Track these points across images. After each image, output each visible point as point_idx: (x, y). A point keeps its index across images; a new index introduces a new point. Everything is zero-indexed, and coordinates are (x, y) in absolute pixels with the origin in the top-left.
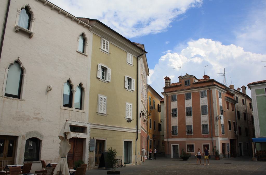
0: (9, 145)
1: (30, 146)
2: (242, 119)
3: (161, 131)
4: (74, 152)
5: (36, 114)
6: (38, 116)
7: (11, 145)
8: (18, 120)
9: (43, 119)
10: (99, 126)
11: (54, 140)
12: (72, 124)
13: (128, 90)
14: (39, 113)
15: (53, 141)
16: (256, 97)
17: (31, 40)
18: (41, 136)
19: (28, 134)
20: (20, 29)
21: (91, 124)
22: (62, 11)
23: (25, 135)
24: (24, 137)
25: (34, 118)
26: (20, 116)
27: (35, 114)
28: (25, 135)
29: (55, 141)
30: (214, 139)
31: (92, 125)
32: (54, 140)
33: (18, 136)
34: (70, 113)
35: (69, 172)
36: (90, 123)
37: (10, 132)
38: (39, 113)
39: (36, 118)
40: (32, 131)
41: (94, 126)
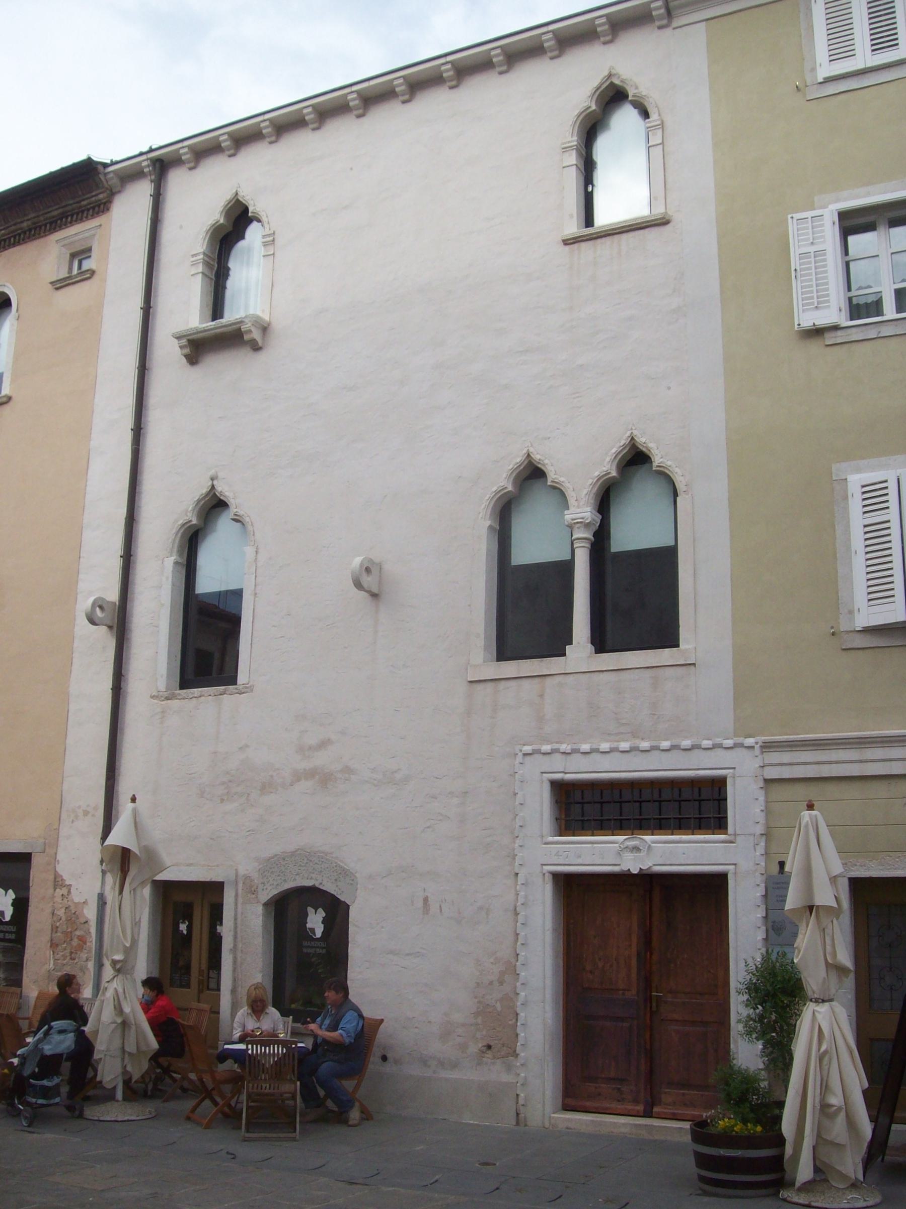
0: (190, 928)
1: (305, 934)
2: (655, 113)
3: (571, 643)
4: (647, 983)
5: (310, 748)
6: (321, 759)
7: (183, 927)
8: (222, 800)
9: (348, 770)
10: (869, 754)
11: (426, 900)
12: (569, 777)
13: (856, 335)
14: (324, 744)
15: (420, 904)
17: (13, 397)
18: (345, 873)
19: (272, 864)
20: (189, 340)
21: (767, 747)
22: (606, 15)
23: (255, 875)
24: (251, 887)
25: (298, 777)
26: (228, 773)
27: (303, 750)
28: (255, 875)
29: (434, 908)
31: (774, 757)
32: (426, 900)
33: (219, 879)
34: (541, 696)
35: (550, 1117)
36: (750, 741)
37: (191, 865)
38: (324, 744)
39: (310, 774)
40: (291, 848)
41: (786, 757)
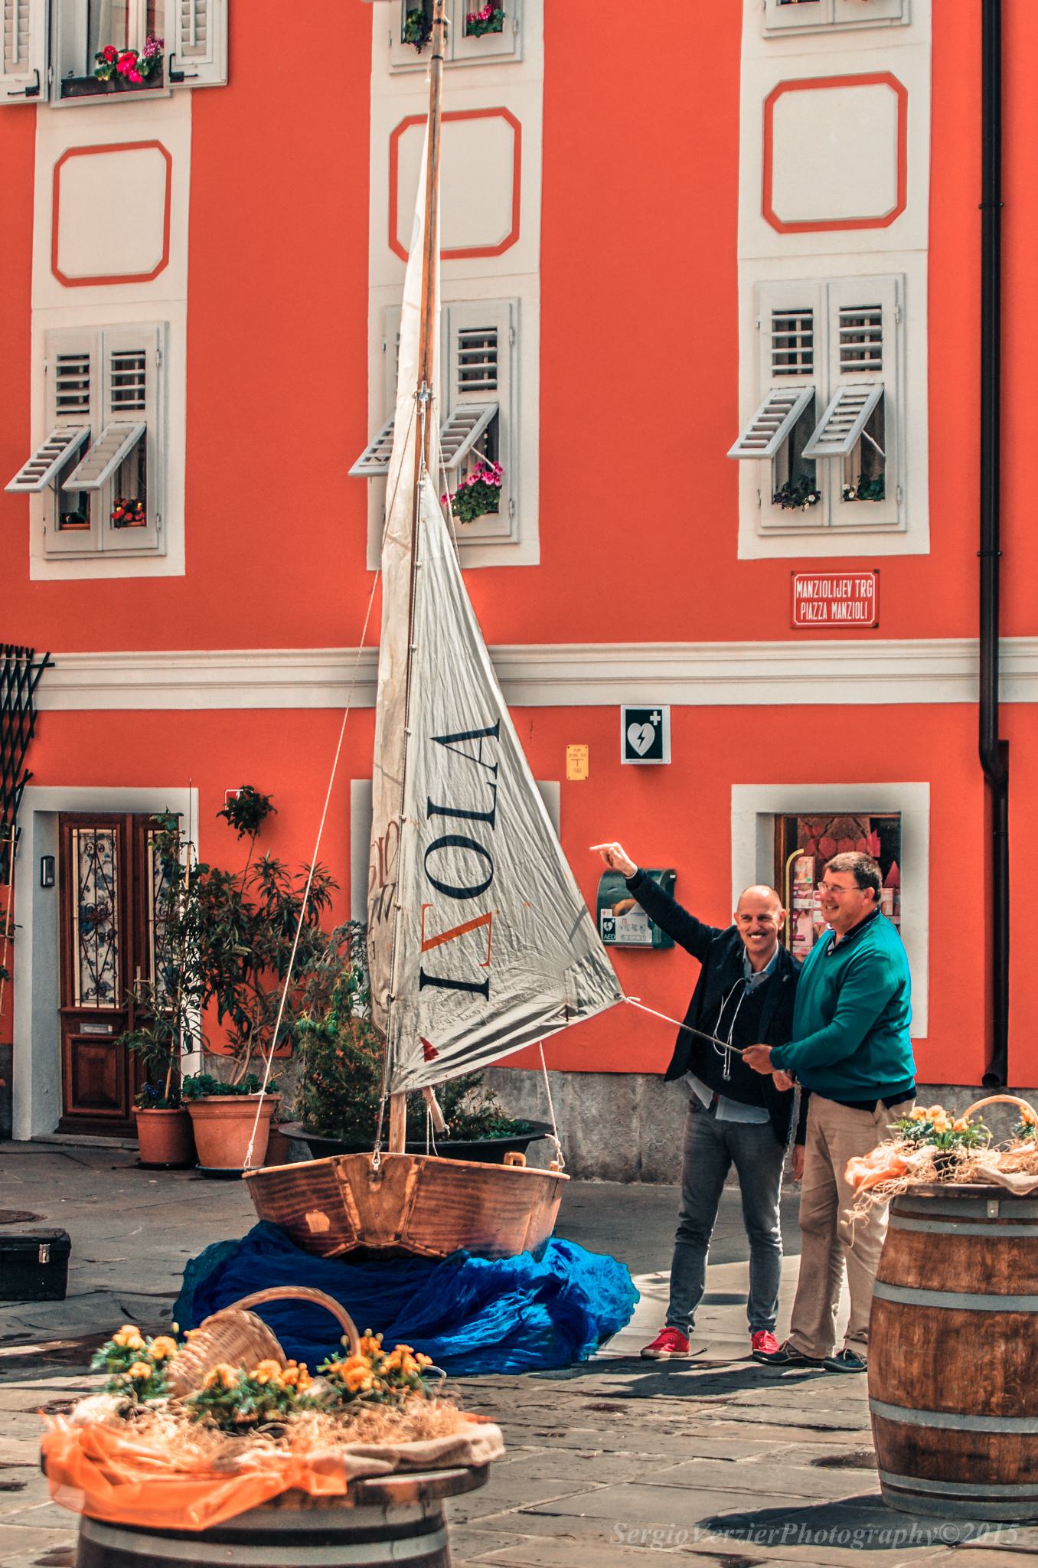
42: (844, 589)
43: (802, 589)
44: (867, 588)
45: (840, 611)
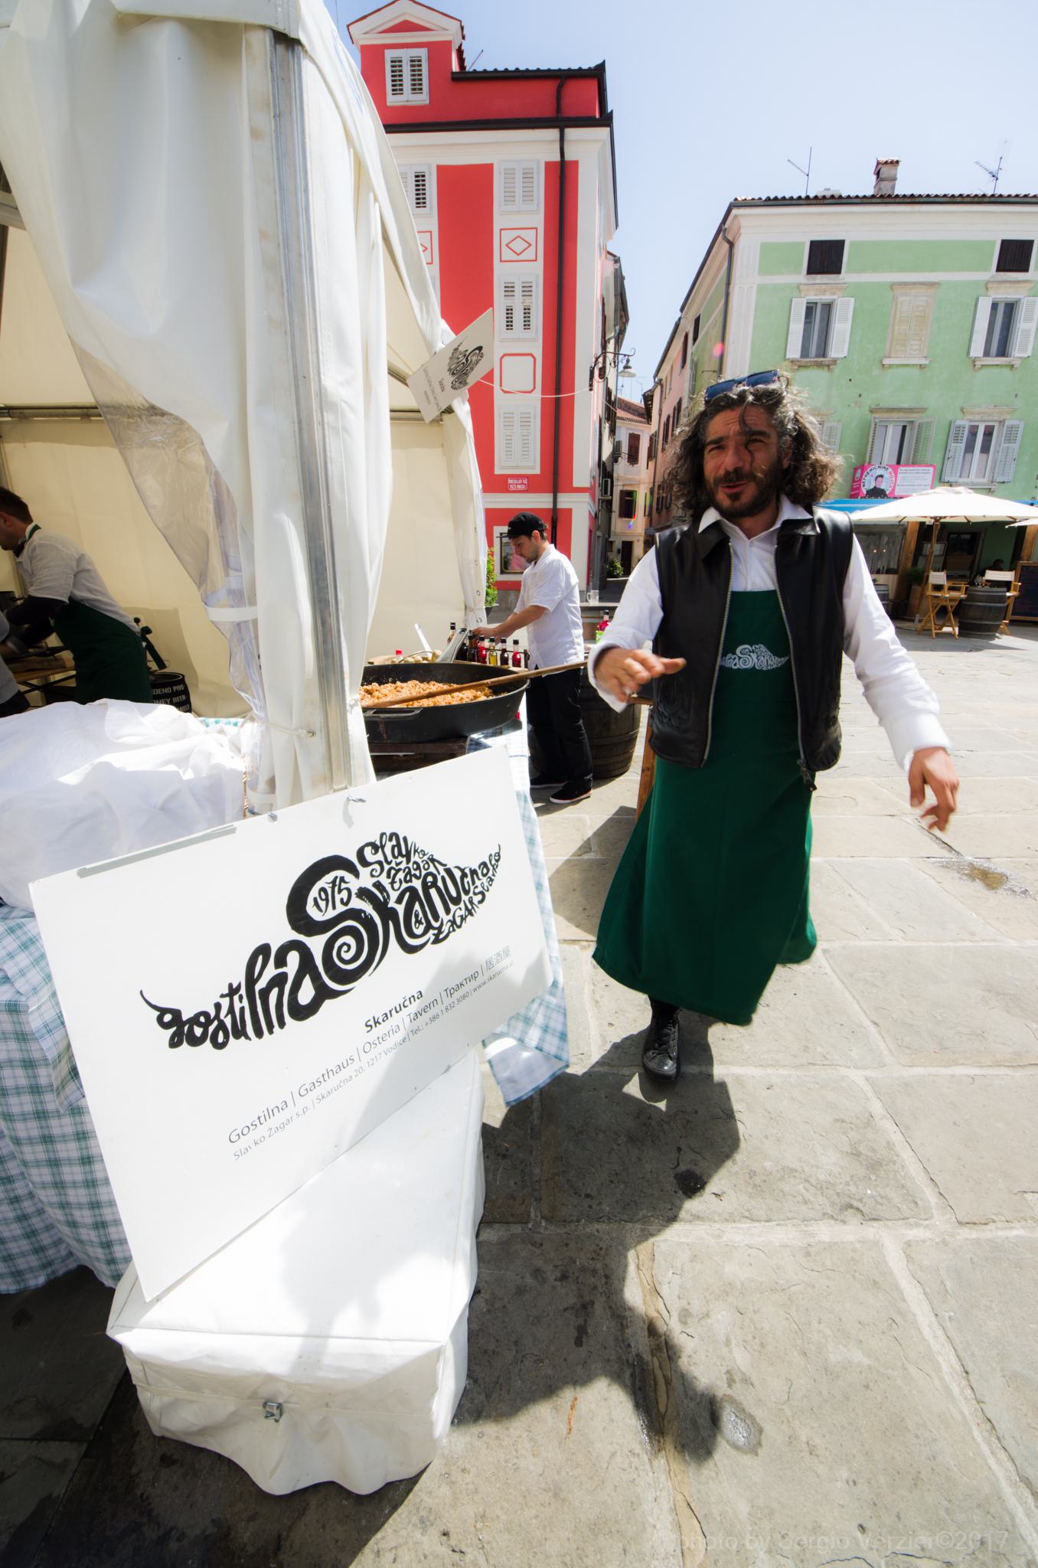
16: (755, 287)
30: (565, 501)
42: (520, 482)
43: (510, 481)
44: (525, 481)
45: (519, 487)
